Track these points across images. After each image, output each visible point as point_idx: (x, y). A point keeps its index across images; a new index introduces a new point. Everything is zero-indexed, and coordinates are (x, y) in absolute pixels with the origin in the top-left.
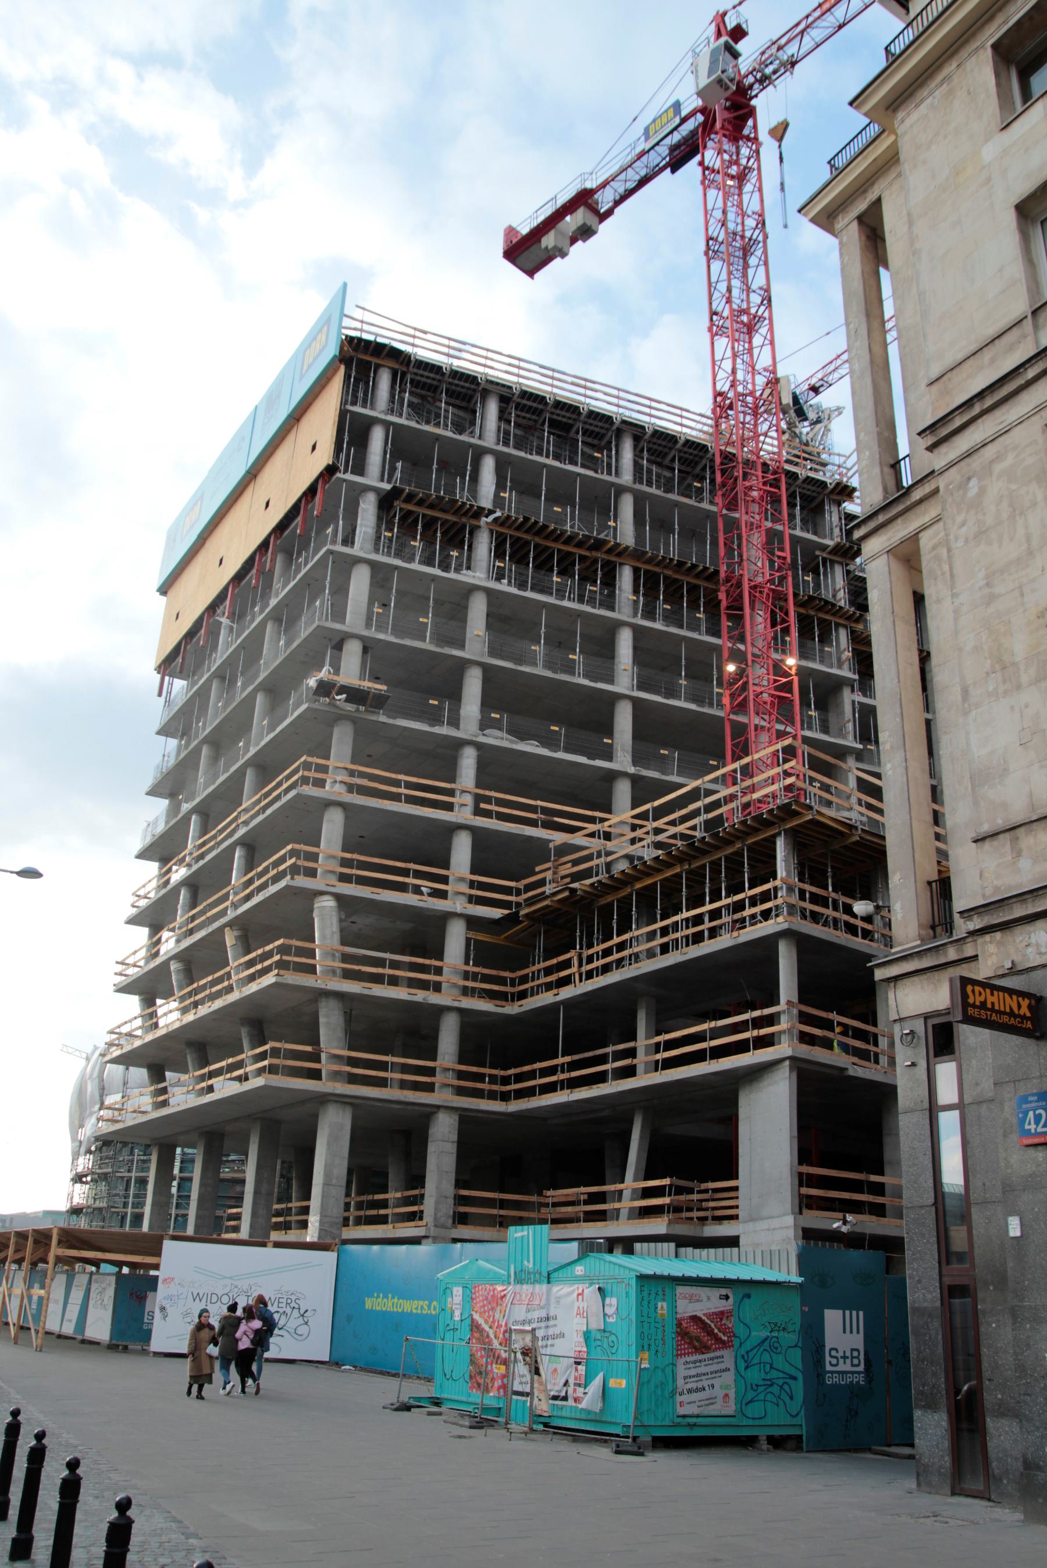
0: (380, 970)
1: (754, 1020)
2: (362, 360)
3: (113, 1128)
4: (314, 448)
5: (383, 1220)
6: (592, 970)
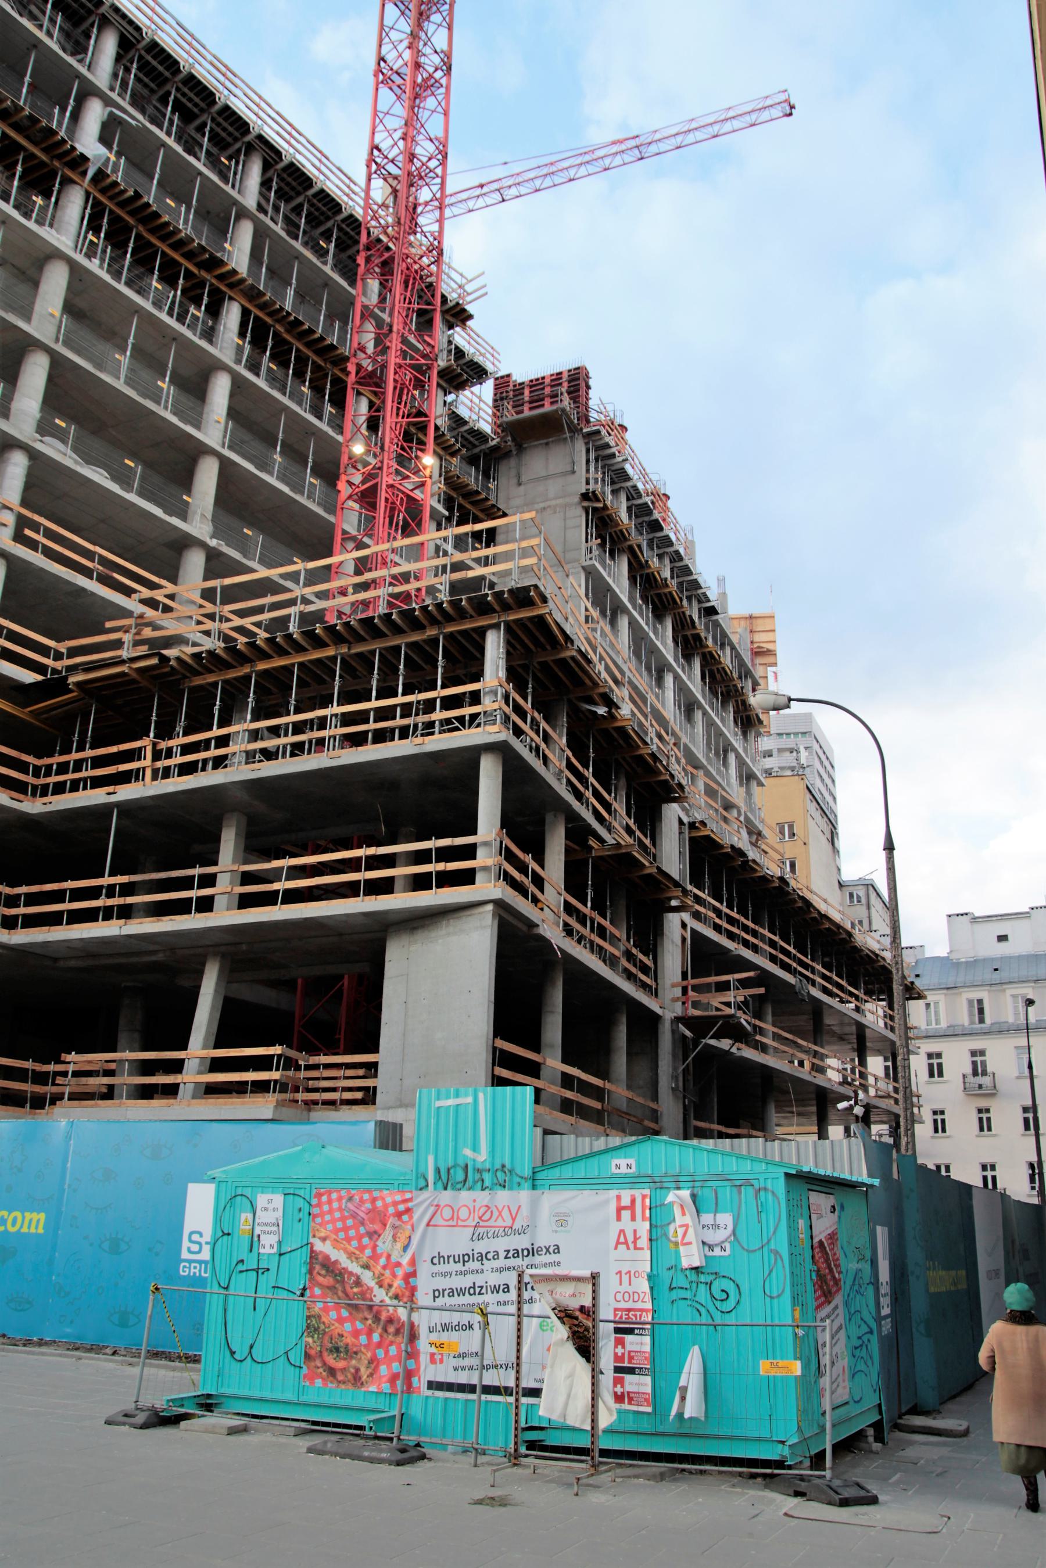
1: (439, 850)
6: (80, 779)
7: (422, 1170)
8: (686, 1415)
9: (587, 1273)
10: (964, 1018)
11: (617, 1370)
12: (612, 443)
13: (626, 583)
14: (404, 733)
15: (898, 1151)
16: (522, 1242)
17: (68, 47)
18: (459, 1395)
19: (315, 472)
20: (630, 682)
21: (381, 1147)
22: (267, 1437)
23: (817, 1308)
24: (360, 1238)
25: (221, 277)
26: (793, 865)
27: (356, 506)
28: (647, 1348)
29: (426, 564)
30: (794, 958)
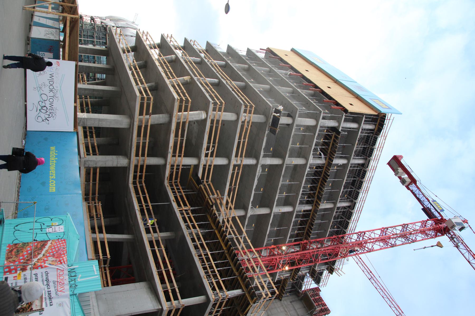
0: (180, 136)
1: (175, 289)
2: (379, 120)
3: (114, 33)
4: (351, 104)
5: (86, 136)
16: (53, 295)
17: (357, 153)
25: (317, 202)
29: (261, 280)
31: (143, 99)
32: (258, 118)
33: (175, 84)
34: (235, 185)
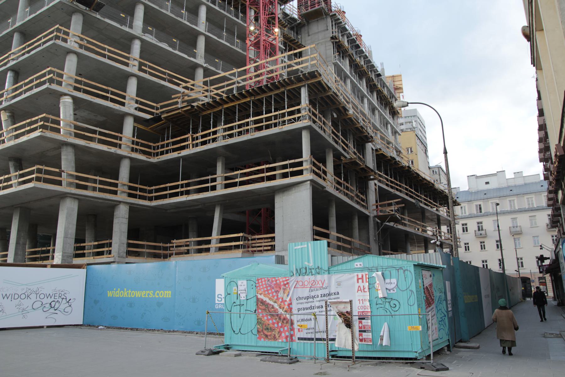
1: (290, 164)
5: (83, 255)
7: (291, 269)
8: (384, 345)
9: (348, 300)
10: (475, 211)
11: (360, 331)
12: (340, 18)
13: (348, 67)
14: (275, 125)
15: (453, 256)
16: (326, 292)
18: (308, 342)
19: (238, 38)
20: (352, 102)
21: (278, 263)
22: (247, 357)
23: (426, 308)
24: (272, 293)
26: (412, 162)
27: (253, 48)
28: (370, 324)
29: (279, 66)
30: (414, 194)
31: (38, 179)
32: (76, 24)
33: (15, 133)
34: (164, 73)
